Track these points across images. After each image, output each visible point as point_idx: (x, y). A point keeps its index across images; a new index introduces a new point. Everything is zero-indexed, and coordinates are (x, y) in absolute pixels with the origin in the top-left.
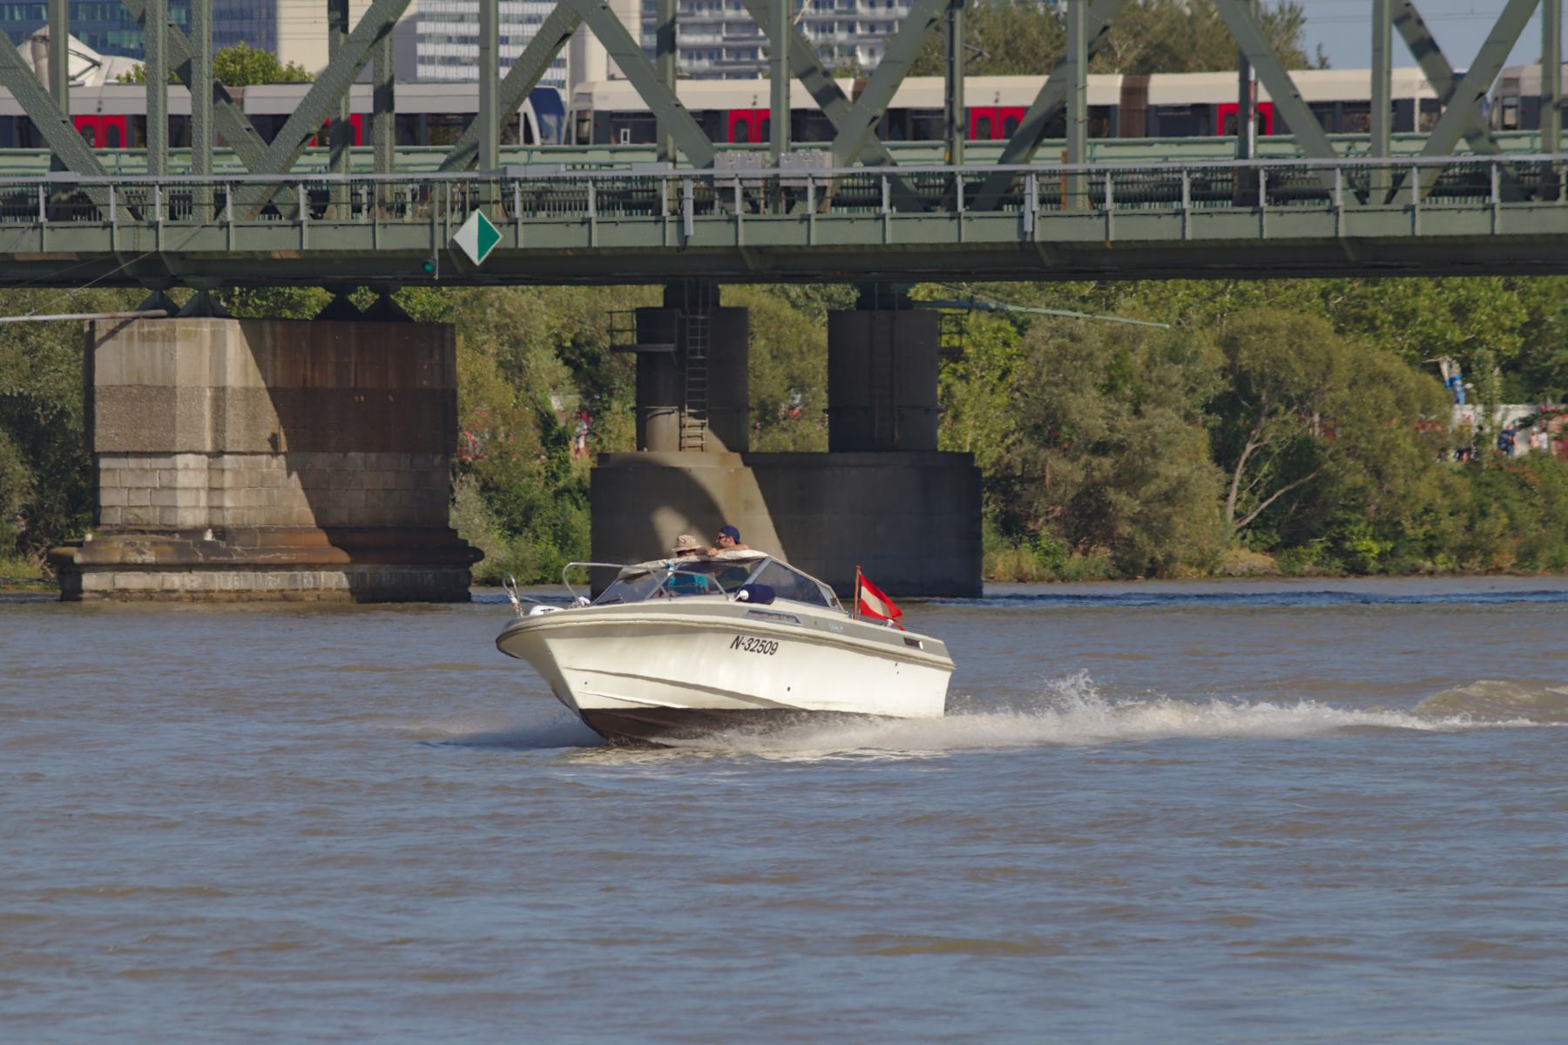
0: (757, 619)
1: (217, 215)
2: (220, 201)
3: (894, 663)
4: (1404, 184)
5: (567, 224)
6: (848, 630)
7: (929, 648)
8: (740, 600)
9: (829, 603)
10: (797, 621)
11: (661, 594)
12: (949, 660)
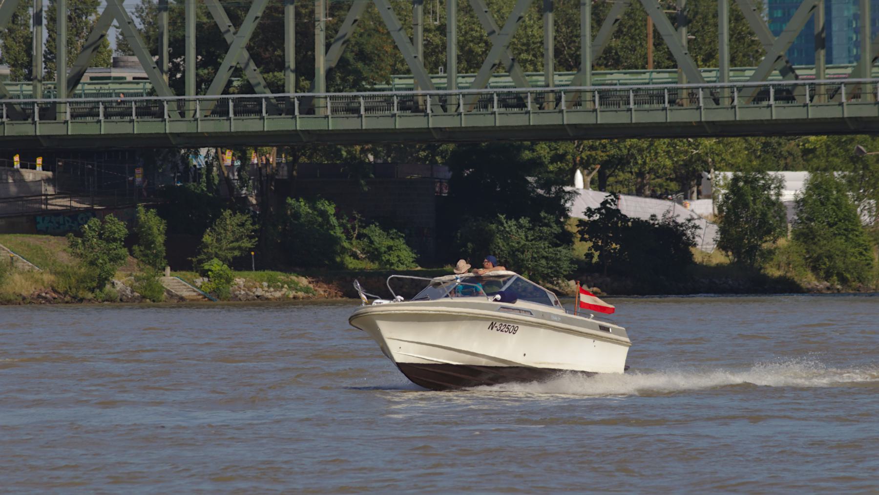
0: (505, 312)
1: (557, 105)
2: (558, 100)
3: (592, 340)
4: (839, 92)
5: (378, 117)
6: (563, 320)
7: (615, 332)
8: (496, 300)
9: (553, 303)
10: (531, 314)
11: (447, 296)
12: (628, 340)
